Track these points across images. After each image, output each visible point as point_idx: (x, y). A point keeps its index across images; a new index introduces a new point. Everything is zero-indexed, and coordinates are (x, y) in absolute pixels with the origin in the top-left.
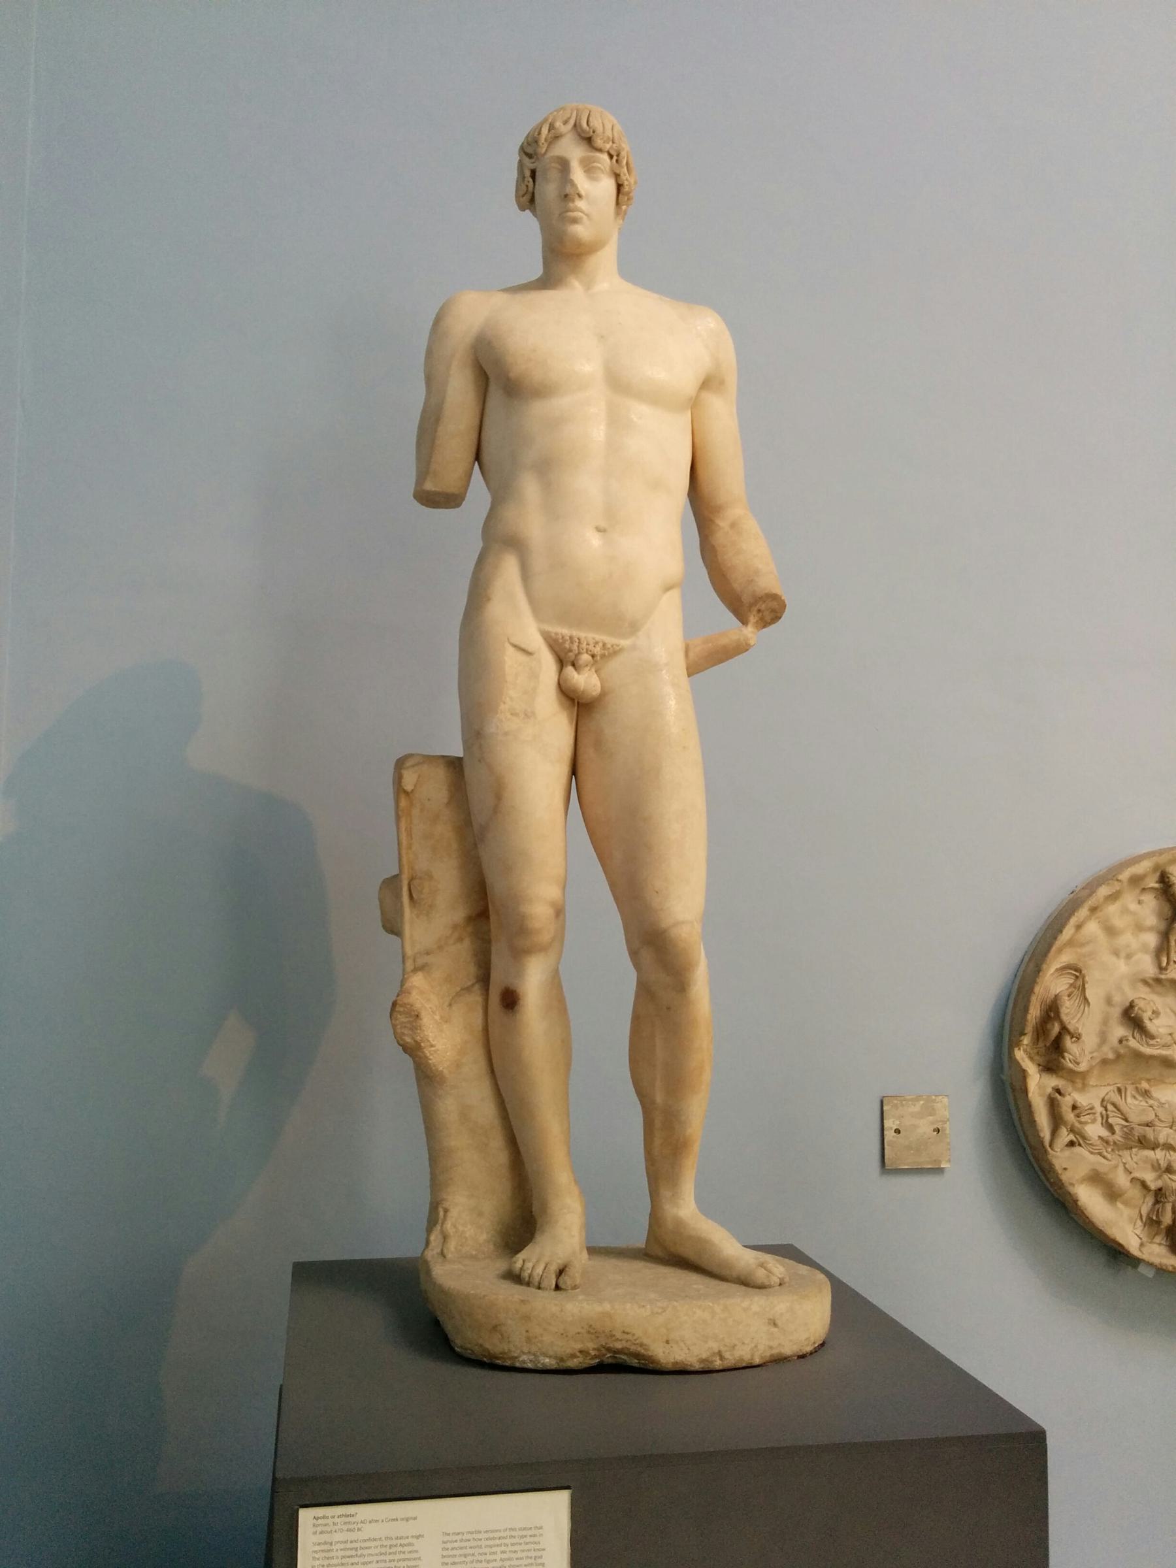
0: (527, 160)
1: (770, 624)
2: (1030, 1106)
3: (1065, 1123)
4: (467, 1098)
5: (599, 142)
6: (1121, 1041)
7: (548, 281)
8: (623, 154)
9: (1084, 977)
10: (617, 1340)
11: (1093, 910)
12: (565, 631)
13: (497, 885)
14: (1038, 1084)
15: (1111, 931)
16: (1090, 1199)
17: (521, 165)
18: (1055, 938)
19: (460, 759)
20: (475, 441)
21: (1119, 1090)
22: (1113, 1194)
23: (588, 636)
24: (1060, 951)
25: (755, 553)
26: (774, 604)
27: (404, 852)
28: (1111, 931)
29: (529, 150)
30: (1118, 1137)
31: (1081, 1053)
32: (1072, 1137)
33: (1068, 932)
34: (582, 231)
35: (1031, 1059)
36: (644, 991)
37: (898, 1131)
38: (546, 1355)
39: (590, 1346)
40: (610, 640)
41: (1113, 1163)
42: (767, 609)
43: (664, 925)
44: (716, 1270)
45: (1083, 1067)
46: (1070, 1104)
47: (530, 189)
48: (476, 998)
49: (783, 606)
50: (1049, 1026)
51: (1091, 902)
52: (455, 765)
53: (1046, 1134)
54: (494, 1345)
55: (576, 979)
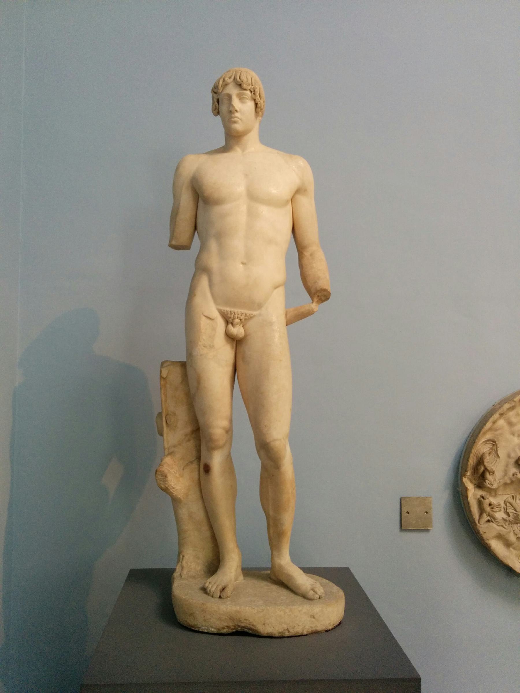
0: (215, 95)
1: (325, 301)
2: (468, 503)
3: (485, 512)
4: (192, 508)
5: (244, 86)
6: (513, 475)
7: (226, 149)
8: (257, 90)
9: (497, 445)
10: (242, 622)
11: (502, 415)
12: (228, 309)
13: (201, 421)
14: (473, 493)
15: (510, 424)
16: (497, 546)
17: (213, 98)
18: (482, 428)
19: (186, 362)
20: (194, 222)
21: (513, 497)
22: (508, 544)
23: (238, 311)
24: (485, 433)
25: (321, 269)
26: (325, 293)
27: (163, 403)
28: (510, 424)
29: (215, 90)
30: (511, 519)
31: (492, 481)
32: (488, 518)
33: (489, 425)
34: (238, 127)
35: (471, 481)
36: (264, 468)
37: (408, 513)
38: (212, 627)
39: (231, 624)
40: (249, 312)
41: (508, 530)
42: (321, 295)
43: (268, 441)
44: (294, 589)
45: (495, 486)
46: (488, 503)
47: (217, 107)
48: (195, 466)
49: (329, 294)
50: (479, 467)
51: (501, 411)
52: (183, 365)
53: (476, 515)
54: (191, 621)
55: (234, 462)
